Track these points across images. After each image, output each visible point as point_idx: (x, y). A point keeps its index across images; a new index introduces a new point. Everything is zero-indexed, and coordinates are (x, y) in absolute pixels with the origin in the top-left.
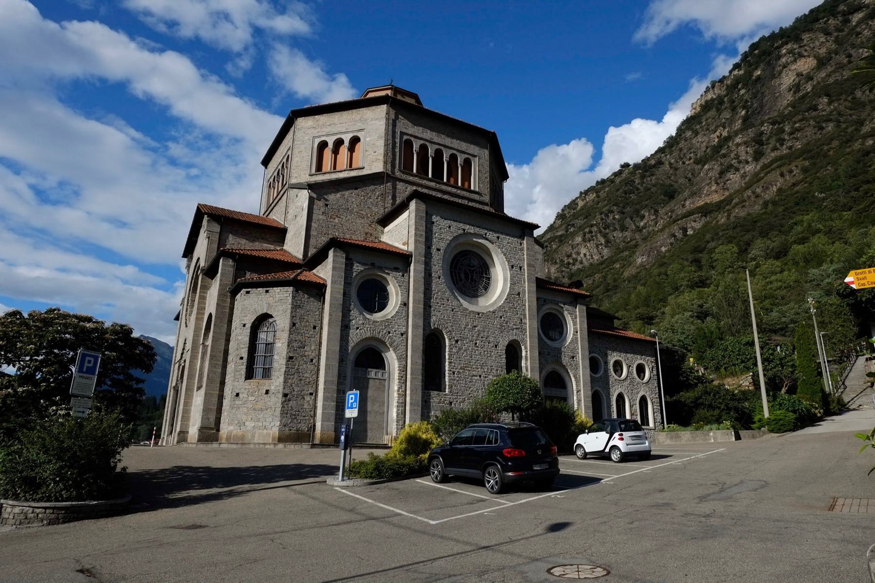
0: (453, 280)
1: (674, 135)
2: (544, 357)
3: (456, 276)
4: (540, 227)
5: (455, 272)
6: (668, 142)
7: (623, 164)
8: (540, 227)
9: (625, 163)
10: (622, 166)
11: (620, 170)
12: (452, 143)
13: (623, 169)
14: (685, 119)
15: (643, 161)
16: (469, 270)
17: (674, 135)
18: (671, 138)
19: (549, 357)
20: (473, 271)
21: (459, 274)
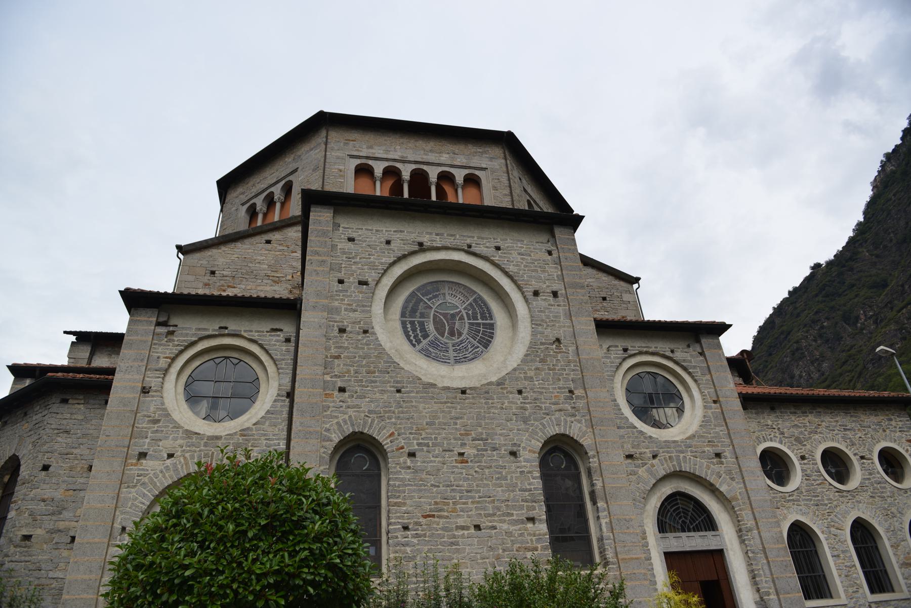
0: (408, 337)
1: (862, 220)
2: (644, 464)
3: (414, 330)
4: (730, 326)
5: (412, 323)
6: (857, 230)
7: (812, 265)
8: (730, 326)
9: (815, 264)
10: (812, 268)
11: (811, 273)
12: (387, 151)
13: (816, 270)
14: (869, 200)
15: (835, 256)
16: (445, 315)
17: (862, 220)
18: (859, 224)
19: (655, 461)
20: (453, 316)
21: (422, 324)
